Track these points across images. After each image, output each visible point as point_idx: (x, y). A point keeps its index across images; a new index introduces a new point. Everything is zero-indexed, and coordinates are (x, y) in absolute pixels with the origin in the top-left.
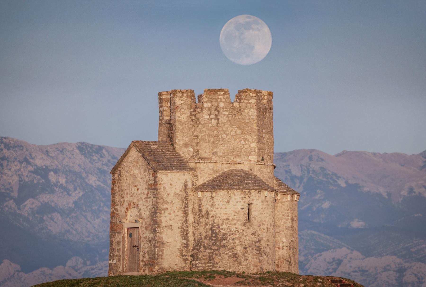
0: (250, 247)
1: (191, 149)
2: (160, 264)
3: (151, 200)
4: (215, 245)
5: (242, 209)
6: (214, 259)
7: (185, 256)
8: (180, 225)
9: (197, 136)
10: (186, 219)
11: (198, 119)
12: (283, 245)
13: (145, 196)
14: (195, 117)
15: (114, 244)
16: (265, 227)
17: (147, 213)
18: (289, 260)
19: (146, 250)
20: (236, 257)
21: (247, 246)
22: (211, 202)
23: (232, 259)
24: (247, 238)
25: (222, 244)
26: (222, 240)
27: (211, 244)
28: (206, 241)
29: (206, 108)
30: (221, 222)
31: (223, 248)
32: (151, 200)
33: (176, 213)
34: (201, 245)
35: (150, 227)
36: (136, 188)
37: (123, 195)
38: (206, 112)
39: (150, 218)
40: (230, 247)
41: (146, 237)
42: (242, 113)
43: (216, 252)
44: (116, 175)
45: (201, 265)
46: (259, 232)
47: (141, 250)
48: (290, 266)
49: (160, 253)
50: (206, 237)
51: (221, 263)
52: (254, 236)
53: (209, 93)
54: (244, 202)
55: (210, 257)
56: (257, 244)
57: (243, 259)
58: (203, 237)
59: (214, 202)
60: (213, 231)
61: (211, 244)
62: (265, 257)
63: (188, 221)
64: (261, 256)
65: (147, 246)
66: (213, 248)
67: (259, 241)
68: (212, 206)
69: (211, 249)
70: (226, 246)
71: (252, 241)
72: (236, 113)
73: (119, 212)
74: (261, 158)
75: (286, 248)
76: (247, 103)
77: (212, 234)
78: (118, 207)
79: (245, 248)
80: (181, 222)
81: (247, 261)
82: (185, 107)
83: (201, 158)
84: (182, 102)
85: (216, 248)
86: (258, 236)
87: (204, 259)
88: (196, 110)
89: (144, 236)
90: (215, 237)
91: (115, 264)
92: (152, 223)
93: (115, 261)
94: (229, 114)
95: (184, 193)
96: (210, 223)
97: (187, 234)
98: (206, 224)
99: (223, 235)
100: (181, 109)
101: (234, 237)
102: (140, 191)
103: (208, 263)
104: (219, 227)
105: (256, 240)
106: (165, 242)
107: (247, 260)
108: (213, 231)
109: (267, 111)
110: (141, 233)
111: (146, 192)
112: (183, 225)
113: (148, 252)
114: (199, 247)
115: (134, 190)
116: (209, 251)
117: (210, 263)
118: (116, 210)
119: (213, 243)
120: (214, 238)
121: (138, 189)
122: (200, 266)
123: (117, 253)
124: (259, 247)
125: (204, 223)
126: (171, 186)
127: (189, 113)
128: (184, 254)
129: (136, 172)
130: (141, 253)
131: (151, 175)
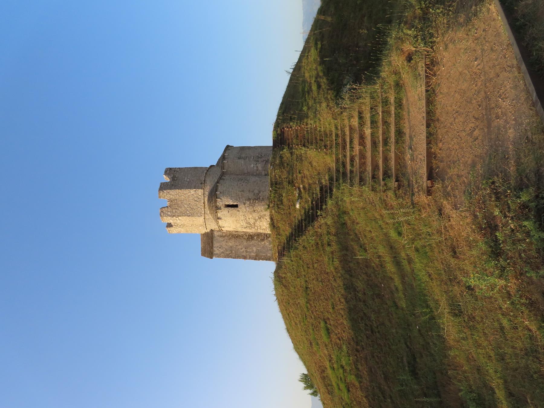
16: (240, 193)
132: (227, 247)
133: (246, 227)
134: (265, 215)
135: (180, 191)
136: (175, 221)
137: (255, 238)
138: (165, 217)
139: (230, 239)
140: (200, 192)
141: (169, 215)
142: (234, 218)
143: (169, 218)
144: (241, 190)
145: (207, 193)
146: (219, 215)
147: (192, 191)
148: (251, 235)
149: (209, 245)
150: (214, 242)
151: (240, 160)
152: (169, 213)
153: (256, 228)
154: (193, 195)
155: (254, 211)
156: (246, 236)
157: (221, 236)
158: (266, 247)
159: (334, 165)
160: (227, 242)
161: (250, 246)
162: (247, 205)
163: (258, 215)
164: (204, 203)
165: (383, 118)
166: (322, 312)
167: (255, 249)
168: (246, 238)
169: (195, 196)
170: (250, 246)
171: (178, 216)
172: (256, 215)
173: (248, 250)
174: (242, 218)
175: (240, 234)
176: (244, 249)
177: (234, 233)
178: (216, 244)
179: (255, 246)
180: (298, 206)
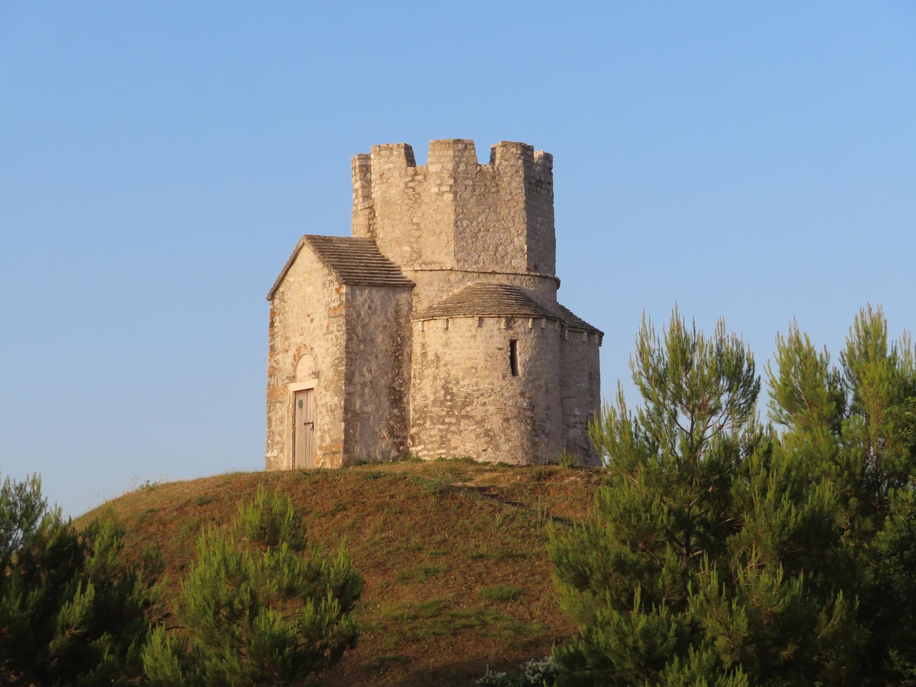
1: (407, 248)
3: (333, 336)
4: (450, 416)
5: (500, 349)
6: (449, 440)
7: (398, 437)
9: (417, 224)
11: (419, 194)
13: (325, 330)
14: (414, 190)
15: (273, 424)
16: (542, 383)
17: (329, 360)
19: (326, 427)
20: (488, 436)
22: (443, 340)
25: (463, 413)
26: (464, 405)
27: (444, 413)
28: (433, 409)
29: (433, 173)
30: (461, 374)
31: (466, 421)
32: (333, 336)
34: (426, 418)
35: (333, 386)
36: (309, 319)
37: (288, 334)
38: (433, 180)
39: (332, 370)
40: (478, 418)
41: (327, 403)
43: (453, 428)
44: (276, 301)
45: (425, 452)
47: (318, 428)
48: (587, 459)
50: (434, 402)
51: (462, 447)
53: (437, 146)
55: (442, 437)
58: (429, 402)
59: (449, 338)
60: (447, 391)
61: (444, 413)
62: (543, 436)
64: (536, 436)
65: (327, 419)
66: (447, 420)
68: (446, 344)
69: (443, 423)
70: (472, 417)
73: (281, 365)
74: (533, 264)
77: (445, 395)
78: (279, 357)
82: (396, 174)
83: (426, 264)
84: (391, 165)
85: (453, 420)
87: (432, 442)
88: (417, 178)
89: (323, 402)
90: (450, 401)
91: (275, 457)
92: (336, 378)
93: (275, 453)
95: (395, 324)
96: (442, 377)
98: (435, 378)
99: (465, 398)
100: (388, 179)
101: (486, 400)
102: (316, 322)
103: (438, 448)
104: (458, 383)
108: (447, 391)
109: (543, 186)
110: (318, 397)
111: (325, 323)
113: (329, 430)
114: (422, 422)
115: (306, 323)
116: (442, 427)
117: (443, 448)
118: (277, 362)
119: (448, 412)
120: (449, 403)
121: (312, 320)
122: (425, 455)
123: (278, 438)
125: (431, 378)
127: (402, 185)
129: (310, 290)
130: (319, 434)
131: (334, 292)
132: (372, 327)
134: (497, 448)
135: (522, 205)
137: (396, 411)
138: (451, 153)
139: (392, 337)
141: (457, 165)
142: (482, 364)
143: (450, 166)
145: (517, 283)
146: (490, 322)
147: (521, 241)
148: (401, 398)
149: (361, 270)
150: (382, 292)
151: (587, 379)
152: (462, 167)
154: (512, 242)
155: (507, 420)
157: (397, 312)
158: (376, 443)
160: (385, 327)
161: (378, 397)
162: (520, 400)
163: (497, 430)
164: (494, 273)
167: (370, 408)
168: (396, 385)
169: (510, 249)
170: (378, 397)
171: (455, 193)
172: (495, 423)
173: (367, 390)
174: (484, 385)
175: (404, 370)
176: (368, 377)
177: (407, 350)
178: (378, 295)
179: (377, 409)
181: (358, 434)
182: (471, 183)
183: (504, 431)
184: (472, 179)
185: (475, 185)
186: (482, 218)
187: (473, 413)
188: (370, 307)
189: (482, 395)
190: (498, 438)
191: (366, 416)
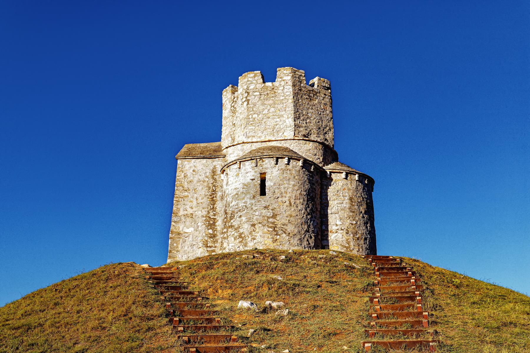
0: (260, 223)
2: (174, 258)
5: (253, 180)
7: (210, 247)
8: (205, 213)
10: (213, 207)
12: (337, 228)
16: (287, 198)
18: (347, 245)
21: (256, 222)
23: (238, 241)
24: (257, 213)
33: (200, 201)
42: (276, 91)
46: (275, 206)
49: (175, 245)
52: (266, 210)
54: (256, 172)
56: (271, 220)
57: (250, 239)
63: (216, 208)
64: (277, 235)
67: (274, 216)
71: (263, 216)
72: (269, 92)
75: (342, 231)
76: (281, 81)
79: (253, 225)
80: (206, 210)
81: (255, 241)
86: (272, 210)
94: (261, 95)
95: (211, 179)
97: (214, 223)
101: (241, 214)
105: (270, 214)
106: (182, 232)
107: (254, 239)
112: (209, 213)
124: (273, 223)
126: (194, 173)
128: (209, 245)
133: (226, 213)
135: (290, 101)
136: (240, 97)
140: (289, 134)
144: (293, 201)
153: (225, 230)
156: (214, 215)
159: (238, 308)
163: (246, 233)
164: (269, 141)
165: (232, 347)
166: (59, 327)
180: (245, 304)
181: (180, 246)
182: (258, 93)
183: (251, 233)
184: (259, 91)
185: (261, 95)
186: (266, 111)
187: (234, 224)
188: (193, 171)
189: (240, 211)
190: (247, 238)
191: (186, 235)
